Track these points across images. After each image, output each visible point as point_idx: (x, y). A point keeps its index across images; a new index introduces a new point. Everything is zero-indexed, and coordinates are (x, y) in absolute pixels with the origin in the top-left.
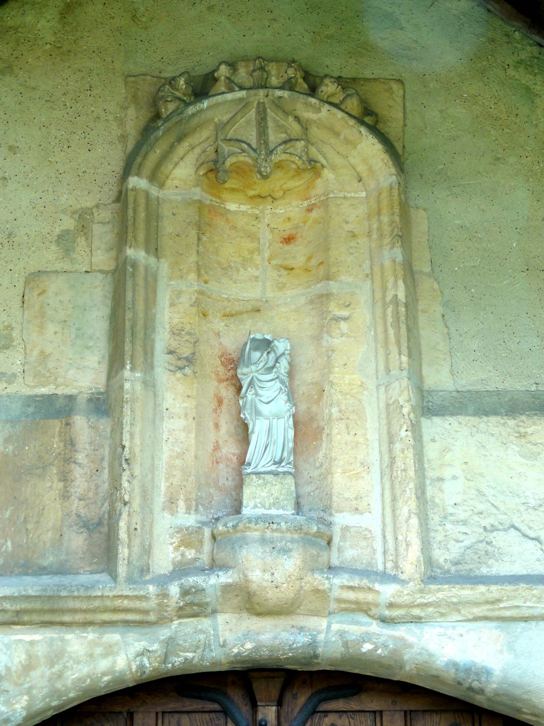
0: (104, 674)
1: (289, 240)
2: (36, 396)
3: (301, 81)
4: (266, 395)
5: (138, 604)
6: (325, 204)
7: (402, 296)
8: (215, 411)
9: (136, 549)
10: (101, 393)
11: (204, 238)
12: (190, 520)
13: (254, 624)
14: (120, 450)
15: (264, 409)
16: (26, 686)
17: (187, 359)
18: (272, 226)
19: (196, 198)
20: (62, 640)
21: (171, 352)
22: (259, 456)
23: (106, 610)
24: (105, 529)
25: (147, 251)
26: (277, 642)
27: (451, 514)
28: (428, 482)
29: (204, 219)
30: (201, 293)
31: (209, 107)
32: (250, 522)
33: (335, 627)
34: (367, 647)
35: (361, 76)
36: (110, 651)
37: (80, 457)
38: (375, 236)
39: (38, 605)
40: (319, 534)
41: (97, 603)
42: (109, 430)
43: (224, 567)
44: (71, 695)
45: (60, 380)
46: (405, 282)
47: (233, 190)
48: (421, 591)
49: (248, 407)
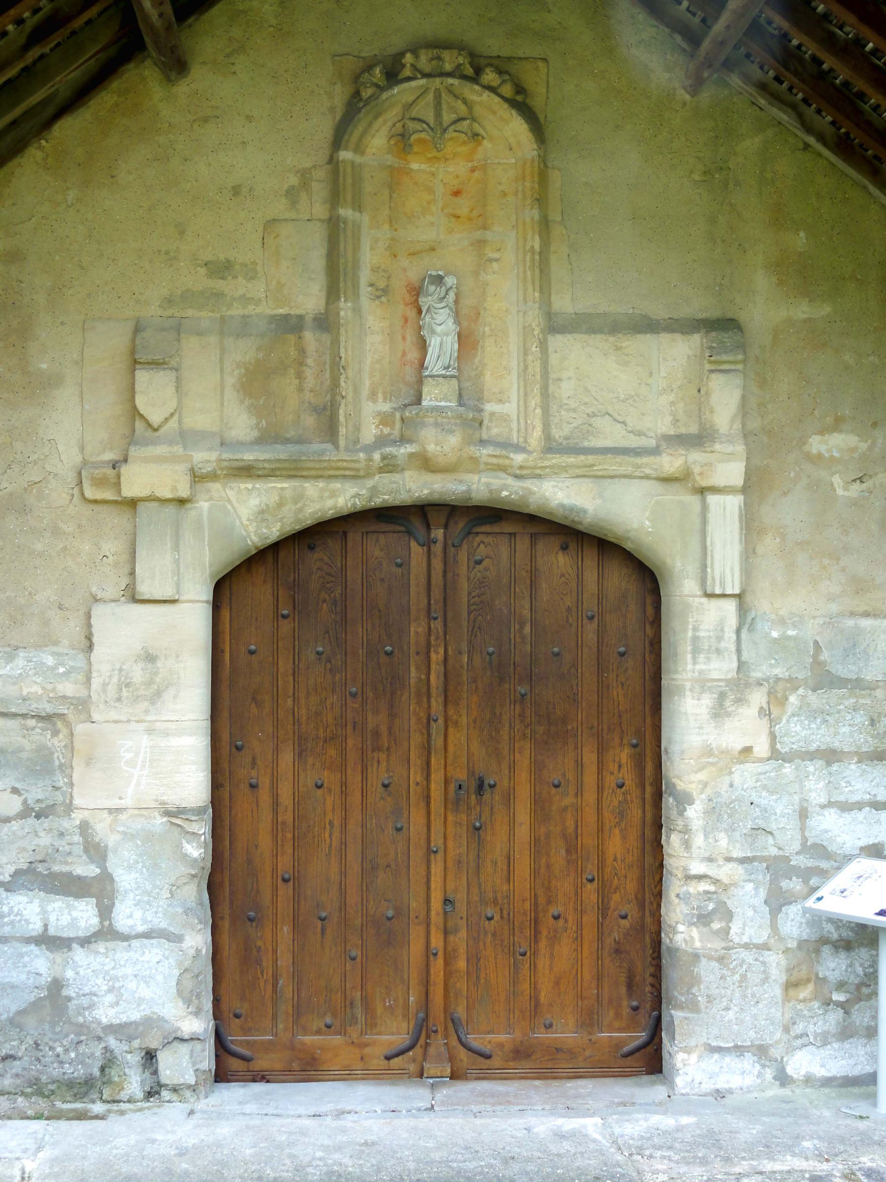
0: (330, 509)
1: (457, 193)
2: (276, 315)
3: (468, 66)
4: (440, 318)
5: (353, 465)
6: (484, 168)
7: (537, 247)
8: (403, 327)
9: (350, 428)
10: (322, 314)
11: (394, 195)
12: (386, 407)
13: (429, 477)
14: (338, 359)
15: (439, 329)
16: (280, 516)
17: (383, 290)
18: (445, 181)
19: (389, 163)
20: (302, 487)
21: (371, 285)
22: (435, 362)
23: (332, 468)
24: (328, 413)
25: (354, 210)
26: (445, 489)
27: (565, 404)
28: (550, 382)
29: (395, 179)
30: (392, 239)
31: (398, 93)
32: (427, 412)
33: (483, 480)
34: (505, 493)
35: (515, 55)
36: (333, 494)
37: (310, 361)
38: (520, 196)
39: (287, 465)
40: (473, 419)
41: (325, 464)
42: (329, 342)
43: (410, 441)
44: (309, 522)
45: (292, 304)
46: (540, 236)
47: (416, 153)
48: (541, 458)
49: (426, 327)
